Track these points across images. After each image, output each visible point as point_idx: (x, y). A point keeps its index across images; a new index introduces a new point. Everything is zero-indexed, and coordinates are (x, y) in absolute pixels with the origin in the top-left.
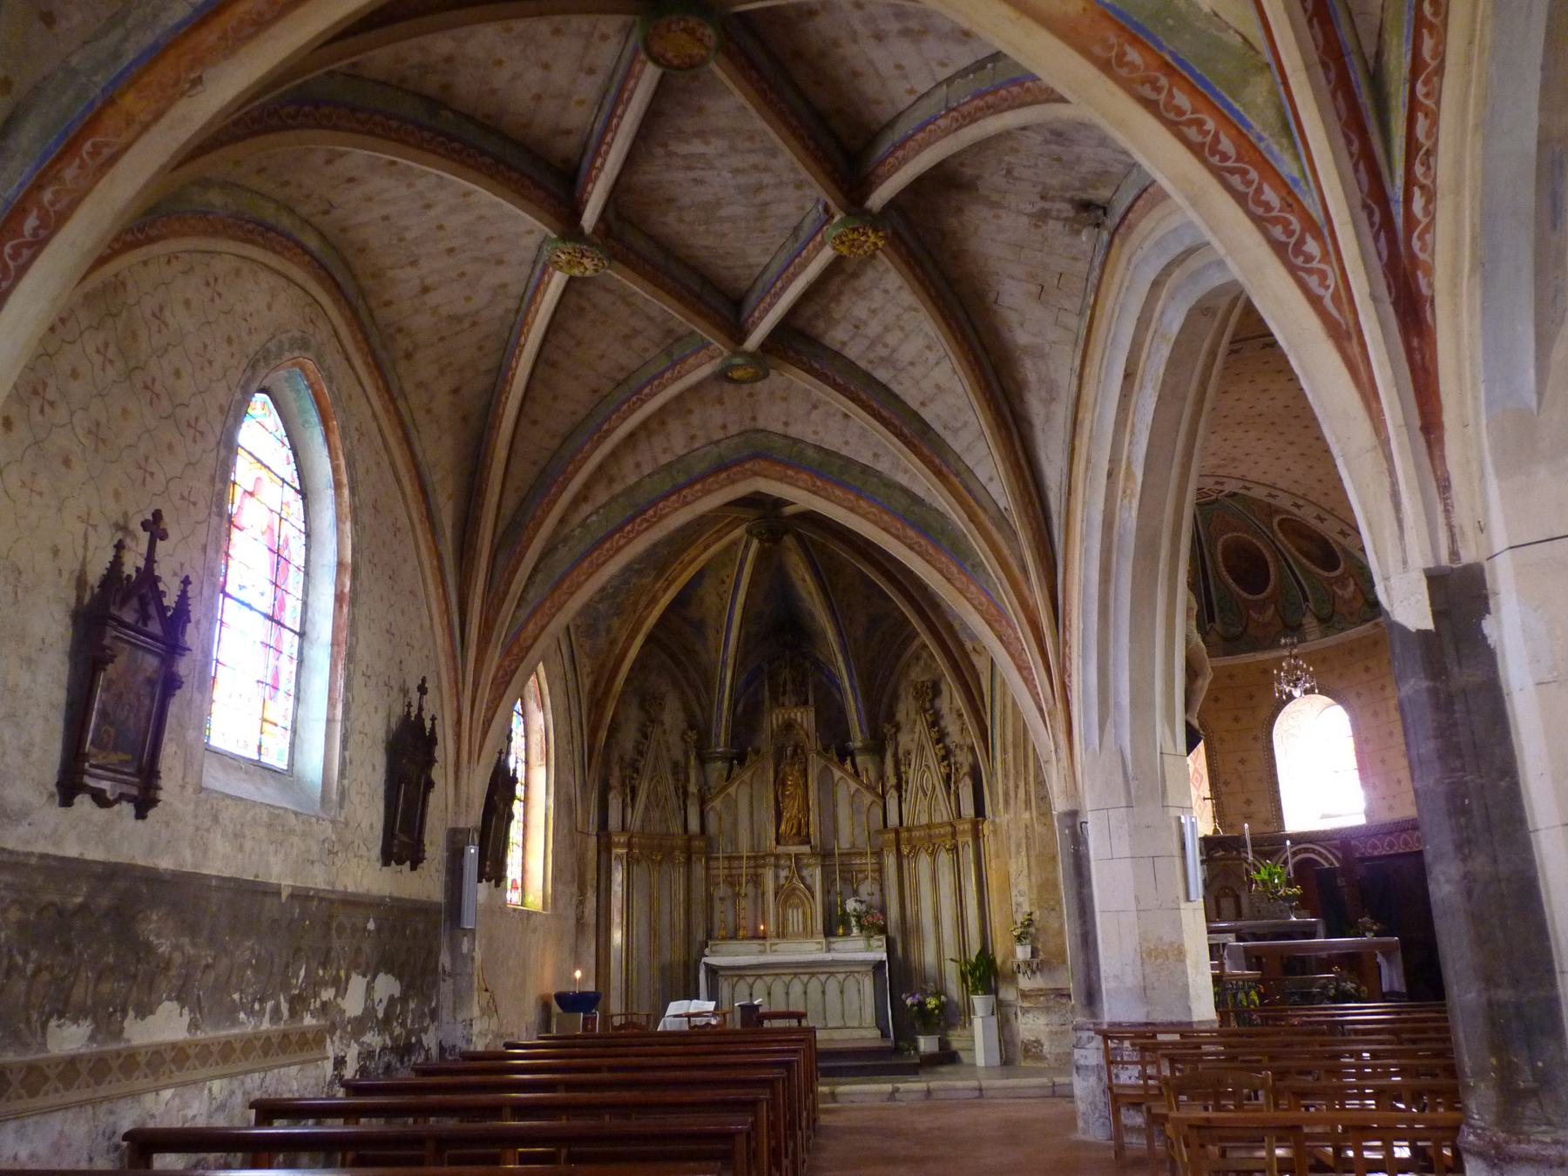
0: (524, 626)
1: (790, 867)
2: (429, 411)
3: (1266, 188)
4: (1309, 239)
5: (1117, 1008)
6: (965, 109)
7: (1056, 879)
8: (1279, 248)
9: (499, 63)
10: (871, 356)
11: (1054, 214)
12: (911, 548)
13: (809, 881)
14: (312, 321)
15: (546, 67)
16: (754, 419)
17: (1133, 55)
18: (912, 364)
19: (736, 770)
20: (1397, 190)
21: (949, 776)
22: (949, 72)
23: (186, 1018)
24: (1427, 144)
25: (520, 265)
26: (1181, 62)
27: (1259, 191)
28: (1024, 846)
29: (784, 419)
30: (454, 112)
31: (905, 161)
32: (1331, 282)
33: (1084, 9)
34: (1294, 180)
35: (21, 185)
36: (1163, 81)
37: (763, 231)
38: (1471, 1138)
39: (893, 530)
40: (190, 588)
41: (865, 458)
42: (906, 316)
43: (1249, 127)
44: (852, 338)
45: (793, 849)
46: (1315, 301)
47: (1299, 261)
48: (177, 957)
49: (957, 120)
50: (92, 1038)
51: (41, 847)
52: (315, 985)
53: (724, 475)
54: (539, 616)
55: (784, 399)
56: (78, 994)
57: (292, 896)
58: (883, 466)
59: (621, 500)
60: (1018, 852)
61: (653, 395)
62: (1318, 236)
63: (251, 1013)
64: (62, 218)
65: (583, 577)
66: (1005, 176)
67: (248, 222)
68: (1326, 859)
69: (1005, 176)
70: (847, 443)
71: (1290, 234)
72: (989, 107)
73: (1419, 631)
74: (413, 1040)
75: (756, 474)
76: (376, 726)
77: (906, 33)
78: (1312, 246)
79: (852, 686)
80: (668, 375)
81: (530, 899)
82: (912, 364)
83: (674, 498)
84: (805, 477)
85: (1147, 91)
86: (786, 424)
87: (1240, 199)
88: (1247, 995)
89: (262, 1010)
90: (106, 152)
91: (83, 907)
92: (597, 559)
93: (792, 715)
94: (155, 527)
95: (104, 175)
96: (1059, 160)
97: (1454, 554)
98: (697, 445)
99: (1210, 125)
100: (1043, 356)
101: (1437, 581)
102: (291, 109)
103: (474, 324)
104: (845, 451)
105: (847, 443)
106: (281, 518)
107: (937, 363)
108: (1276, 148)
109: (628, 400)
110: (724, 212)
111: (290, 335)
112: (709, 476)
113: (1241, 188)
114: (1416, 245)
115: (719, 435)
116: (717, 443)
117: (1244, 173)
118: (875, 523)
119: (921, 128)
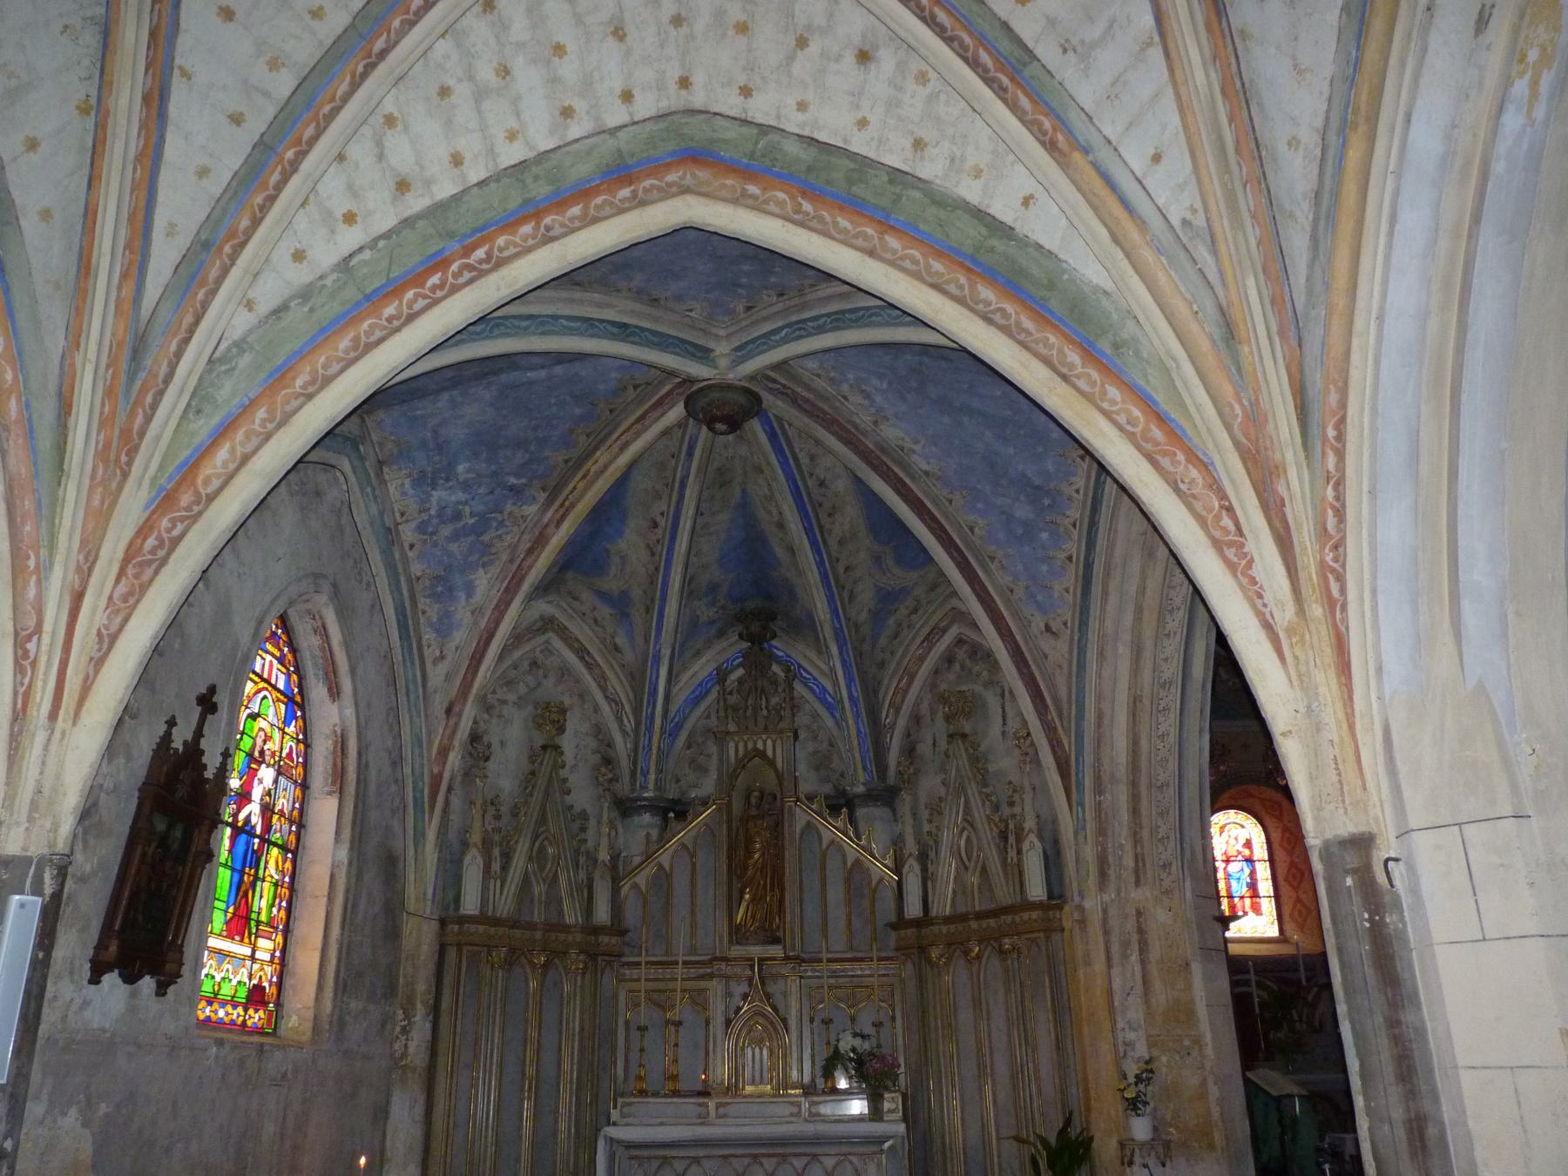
1: (750, 979)
7: (1192, 1001)
12: (988, 320)
13: (778, 999)
16: (684, 83)
19: (674, 825)
29: (742, 80)
39: (952, 289)
40: (174, 730)
45: (756, 951)
54: (240, 435)
55: (742, 28)
58: (931, 169)
59: (421, 224)
60: (1125, 957)
65: (336, 367)
70: (862, 123)
75: (686, 190)
79: (851, 697)
84: (781, 195)
86: (746, 92)
92: (367, 334)
93: (760, 746)
98: (575, 131)
116: (613, 131)
118: (917, 276)
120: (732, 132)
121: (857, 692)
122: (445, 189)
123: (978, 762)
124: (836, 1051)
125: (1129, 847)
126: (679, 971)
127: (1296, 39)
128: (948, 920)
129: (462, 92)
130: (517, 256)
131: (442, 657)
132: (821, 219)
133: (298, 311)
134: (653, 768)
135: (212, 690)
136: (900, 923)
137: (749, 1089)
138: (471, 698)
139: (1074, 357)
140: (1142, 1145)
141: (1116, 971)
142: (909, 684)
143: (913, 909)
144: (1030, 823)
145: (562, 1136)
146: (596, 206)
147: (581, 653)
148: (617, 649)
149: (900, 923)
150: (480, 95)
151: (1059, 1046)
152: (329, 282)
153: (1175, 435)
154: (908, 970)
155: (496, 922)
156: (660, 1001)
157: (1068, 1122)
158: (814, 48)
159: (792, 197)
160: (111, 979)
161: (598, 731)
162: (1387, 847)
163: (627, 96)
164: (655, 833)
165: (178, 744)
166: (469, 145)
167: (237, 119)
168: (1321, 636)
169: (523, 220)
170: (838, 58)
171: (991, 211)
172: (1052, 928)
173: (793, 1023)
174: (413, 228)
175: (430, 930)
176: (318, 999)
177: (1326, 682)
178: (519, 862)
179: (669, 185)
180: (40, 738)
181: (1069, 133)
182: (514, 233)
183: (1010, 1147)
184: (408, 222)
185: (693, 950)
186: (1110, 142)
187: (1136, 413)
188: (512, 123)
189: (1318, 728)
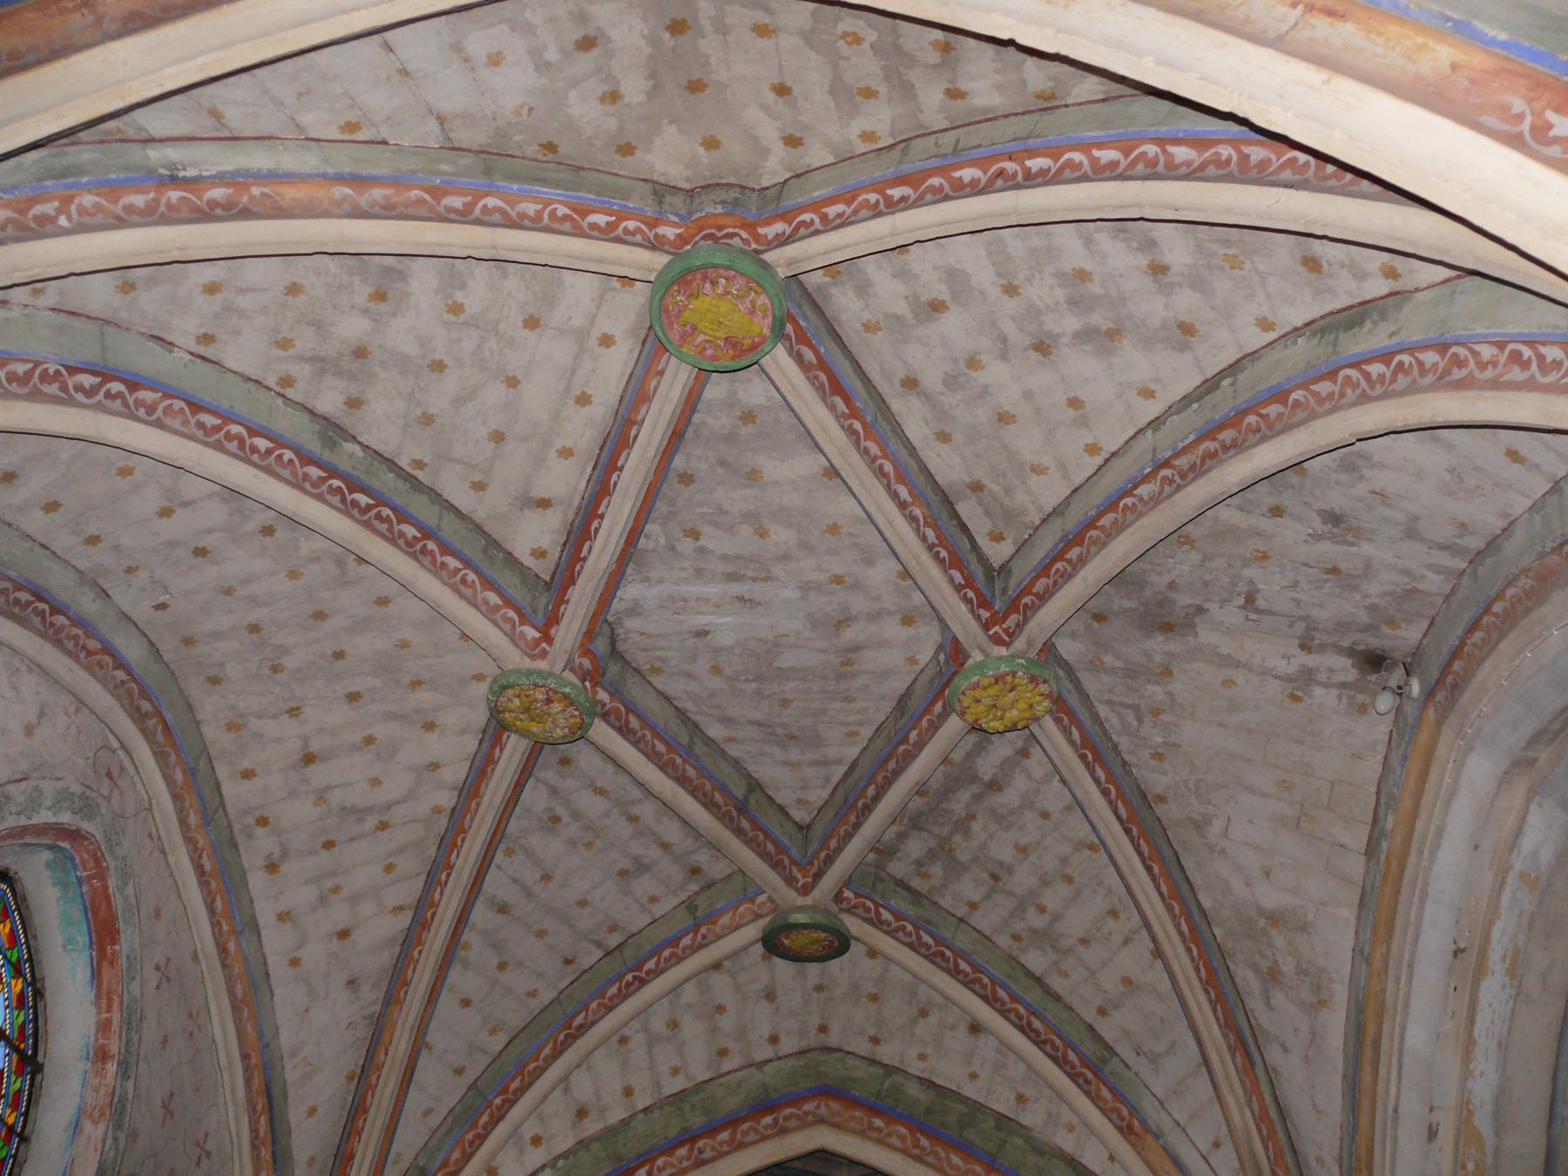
2: (295, 962)
9: (438, 367)
10: (1018, 926)
11: (1323, 677)
14: (109, 775)
15: (513, 382)
16: (823, 1029)
18: (1084, 941)
22: (1154, 409)
25: (463, 732)
29: (872, 1032)
30: (366, 447)
37: (848, 699)
41: (1002, 1103)
44: (988, 896)
49: (1172, 482)
53: (768, 1120)
55: (874, 998)
58: (1032, 1118)
59: (595, 1146)
61: (657, 972)
66: (1243, 607)
67: (19, 587)
69: (1243, 607)
72: (1226, 449)
75: (821, 1121)
77: (1086, 335)
80: (686, 941)
82: (1084, 941)
83: (682, 1151)
84: (903, 1130)
86: (875, 1041)
96: (1334, 571)
98: (727, 1065)
100: (1304, 928)
102: (87, 380)
103: (383, 826)
104: (969, 1090)
107: (1126, 942)
111: (60, 785)
112: (744, 1120)
115: (766, 1052)
116: (761, 1065)
119: (1112, 505)
120: (862, 1071)
122: (616, 1115)
127: (1313, 1087)
129: (638, 1041)
132: (936, 1154)
146: (743, 1132)
150: (652, 1041)
158: (933, 1018)
159: (913, 1133)
166: (640, 1080)
167: (459, 1071)
169: (680, 1144)
170: (953, 1027)
171: (1083, 1161)
174: (588, 1150)
179: (806, 1114)
181: (1143, 1122)
182: (671, 1155)
184: (583, 1144)
186: (1178, 1124)
188: (676, 1062)
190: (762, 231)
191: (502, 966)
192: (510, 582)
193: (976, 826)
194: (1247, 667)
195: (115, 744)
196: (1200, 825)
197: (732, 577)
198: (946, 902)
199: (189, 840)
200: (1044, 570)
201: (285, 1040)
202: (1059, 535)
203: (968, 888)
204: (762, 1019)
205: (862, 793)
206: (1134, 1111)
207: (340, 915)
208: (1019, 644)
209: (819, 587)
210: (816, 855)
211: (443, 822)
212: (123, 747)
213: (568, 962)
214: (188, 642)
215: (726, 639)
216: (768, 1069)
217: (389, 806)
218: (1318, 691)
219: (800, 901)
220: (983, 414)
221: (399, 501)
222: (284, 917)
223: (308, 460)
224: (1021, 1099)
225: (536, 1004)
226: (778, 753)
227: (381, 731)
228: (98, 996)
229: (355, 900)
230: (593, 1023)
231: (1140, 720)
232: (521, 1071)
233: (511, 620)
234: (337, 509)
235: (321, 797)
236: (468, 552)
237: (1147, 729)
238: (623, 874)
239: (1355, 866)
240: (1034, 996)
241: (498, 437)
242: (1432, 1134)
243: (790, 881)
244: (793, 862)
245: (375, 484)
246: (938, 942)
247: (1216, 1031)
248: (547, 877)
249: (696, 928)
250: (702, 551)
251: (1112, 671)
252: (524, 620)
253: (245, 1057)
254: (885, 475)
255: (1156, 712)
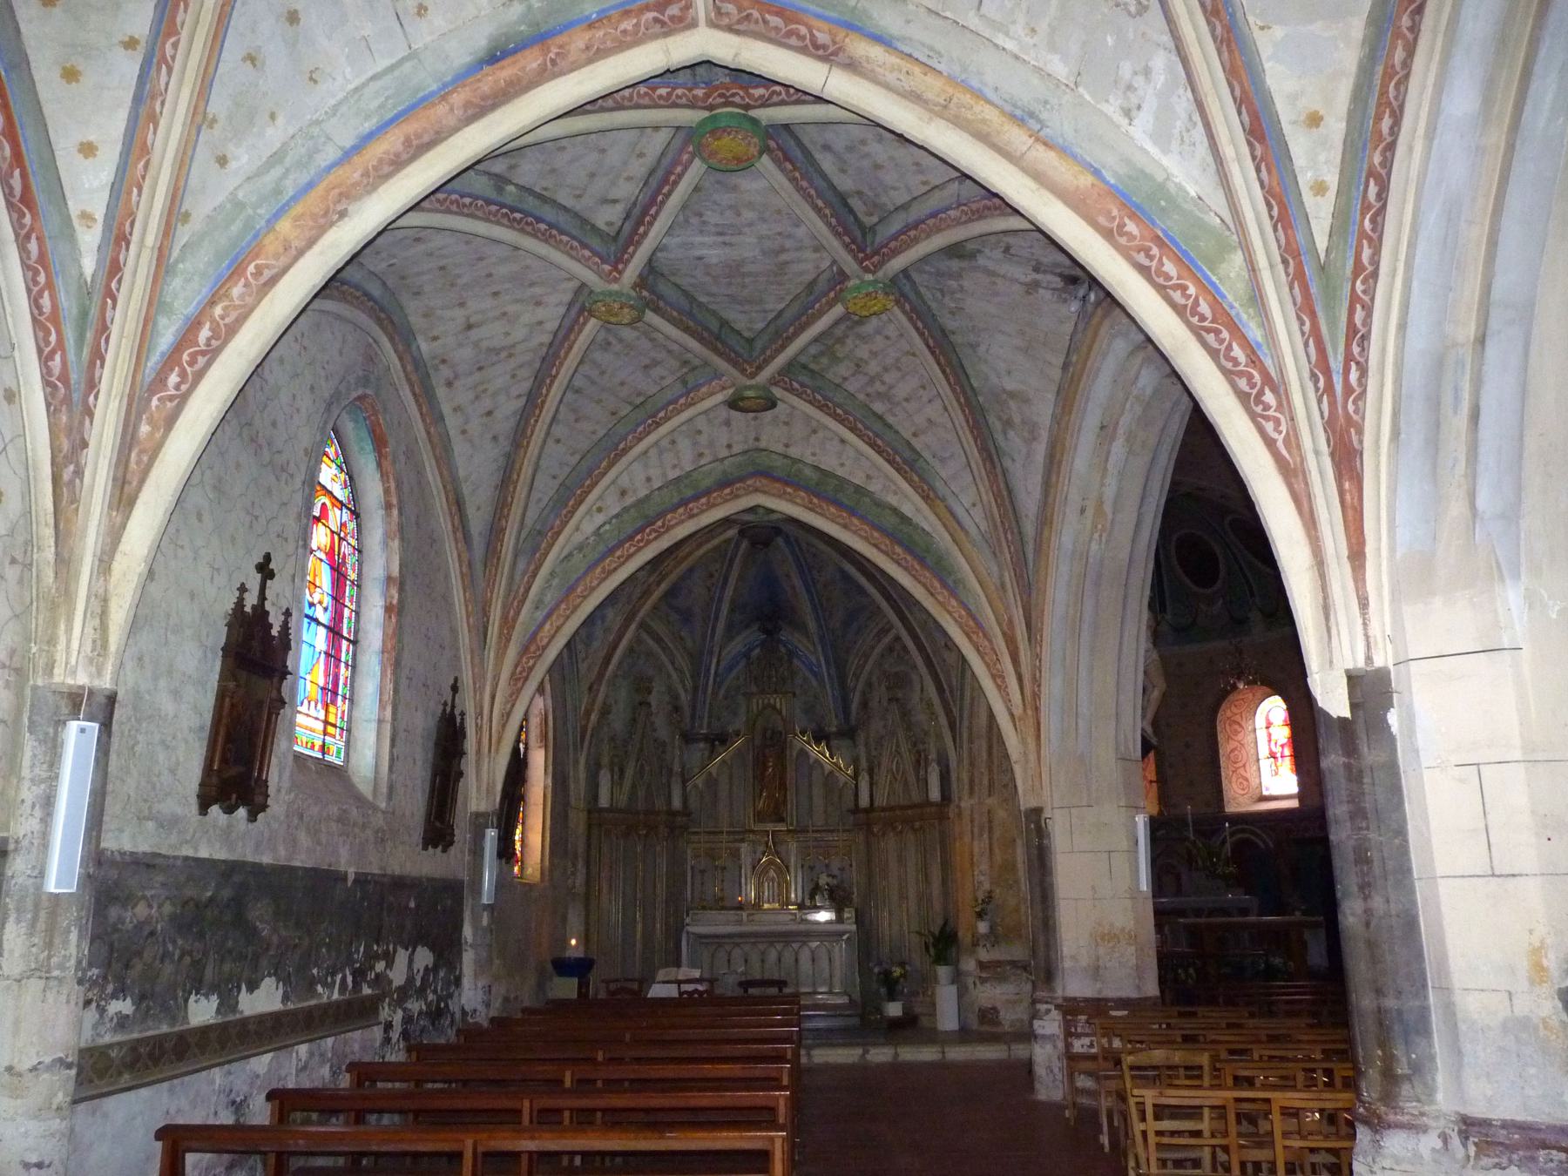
0: (541, 626)
1: (767, 843)
2: (464, 432)
3: (1235, 345)
4: (1267, 391)
5: (1075, 986)
6: (974, 206)
8: (1243, 397)
10: (869, 390)
16: (757, 439)
17: (1131, 227)
18: (907, 400)
20: (1336, 364)
21: (918, 762)
23: (281, 991)
24: (1363, 331)
26: (1167, 236)
27: (1229, 348)
28: (987, 829)
30: (516, 185)
31: (916, 240)
32: (1283, 428)
33: (1093, 185)
34: (1257, 343)
35: (198, 304)
36: (1155, 251)
37: (780, 284)
38: (1361, 1110)
39: (883, 547)
41: (858, 479)
42: (904, 360)
43: (1224, 297)
44: (853, 375)
45: (770, 827)
46: (1270, 443)
47: (1259, 409)
48: (275, 939)
50: (218, 1011)
51: (187, 851)
52: (372, 957)
53: (727, 491)
54: (554, 617)
55: (786, 424)
56: (209, 973)
57: (356, 881)
58: (874, 487)
59: (632, 510)
61: (667, 419)
62: (1274, 390)
63: (325, 985)
64: (232, 330)
65: (596, 582)
68: (1264, 842)
70: (842, 465)
71: (1253, 386)
73: (1339, 718)
74: (442, 1005)
75: (757, 490)
76: (423, 723)
78: (1269, 397)
79: (829, 674)
80: (682, 401)
81: (529, 871)
82: (907, 400)
83: (681, 510)
84: (802, 494)
85: (1141, 258)
86: (787, 446)
87: (1213, 354)
88: (1186, 971)
89: (334, 982)
90: (267, 274)
91: (211, 899)
93: (772, 701)
94: (265, 570)
95: (266, 294)
97: (1369, 659)
98: (702, 462)
99: (1192, 290)
101: (1353, 679)
103: (510, 356)
105: (842, 465)
106: (340, 539)
107: (930, 401)
108: (1245, 317)
109: (644, 422)
110: (745, 270)
113: (1215, 345)
114: (1351, 408)
115: (724, 453)
116: (723, 459)
117: (1217, 332)
119: (934, 215)
120: (779, 462)
121: (833, 671)
122: (643, 493)
123: (906, 714)
124: (817, 884)
125: (986, 773)
126: (725, 835)
128: (883, 809)
130: (677, 524)
131: (587, 657)
133: (578, 557)
134: (706, 715)
135: (268, 558)
136: (856, 810)
137: (766, 906)
138: (604, 682)
139: (937, 584)
140: (985, 935)
141: (976, 843)
142: (866, 662)
143: (864, 801)
144: (933, 756)
145: (658, 932)
147: (659, 640)
148: (682, 638)
149: (856, 810)
151: (944, 882)
152: (591, 541)
153: (979, 626)
154: (861, 838)
155: (620, 811)
156: (712, 855)
157: (945, 924)
158: (820, 434)
160: (215, 810)
161: (671, 690)
162: (1047, 814)
163: (729, 446)
164: (707, 753)
165: (248, 609)
166: (654, 472)
168: (1031, 721)
172: (942, 817)
173: (792, 870)
175: (583, 816)
176: (542, 860)
177: (1031, 741)
178: (629, 772)
180: (486, 760)
183: (915, 939)
184: (626, 510)
185: (731, 825)
187: (963, 613)
189: (1027, 762)
190: (752, 91)
191: (577, 421)
192: (595, 242)
193: (849, 341)
194: (1004, 277)
195: (371, 340)
196: (974, 346)
197: (721, 234)
198: (829, 376)
199: (409, 380)
200: (895, 237)
201: (461, 473)
202: (903, 224)
203: (843, 370)
204: (723, 437)
205: (786, 330)
206: (932, 488)
207: (487, 403)
208: (880, 274)
209: (769, 237)
210: (758, 357)
211: (545, 349)
212: (375, 341)
213: (613, 414)
214: (403, 278)
215: (714, 261)
216: (726, 462)
217: (513, 346)
218: (1041, 291)
219: (749, 382)
220: (866, 163)
221: (538, 213)
222: (456, 409)
223: (488, 202)
224: (868, 477)
225: (595, 438)
226: (738, 307)
227: (511, 309)
228: (382, 476)
229: (495, 394)
230: (631, 448)
231: (943, 296)
232: (590, 473)
233: (596, 263)
234: (507, 227)
235: (476, 344)
236: (574, 232)
237: (947, 300)
238: (646, 367)
239: (1056, 374)
240: (878, 426)
241: (592, 175)
242: (1083, 511)
243: (743, 371)
244: (745, 361)
245: (525, 207)
246: (825, 398)
247: (977, 454)
248: (603, 373)
249: (688, 393)
250: (704, 223)
251: (930, 273)
252: (604, 261)
253: (444, 487)
254: (811, 196)
255: (953, 293)
